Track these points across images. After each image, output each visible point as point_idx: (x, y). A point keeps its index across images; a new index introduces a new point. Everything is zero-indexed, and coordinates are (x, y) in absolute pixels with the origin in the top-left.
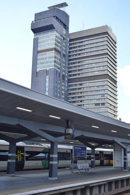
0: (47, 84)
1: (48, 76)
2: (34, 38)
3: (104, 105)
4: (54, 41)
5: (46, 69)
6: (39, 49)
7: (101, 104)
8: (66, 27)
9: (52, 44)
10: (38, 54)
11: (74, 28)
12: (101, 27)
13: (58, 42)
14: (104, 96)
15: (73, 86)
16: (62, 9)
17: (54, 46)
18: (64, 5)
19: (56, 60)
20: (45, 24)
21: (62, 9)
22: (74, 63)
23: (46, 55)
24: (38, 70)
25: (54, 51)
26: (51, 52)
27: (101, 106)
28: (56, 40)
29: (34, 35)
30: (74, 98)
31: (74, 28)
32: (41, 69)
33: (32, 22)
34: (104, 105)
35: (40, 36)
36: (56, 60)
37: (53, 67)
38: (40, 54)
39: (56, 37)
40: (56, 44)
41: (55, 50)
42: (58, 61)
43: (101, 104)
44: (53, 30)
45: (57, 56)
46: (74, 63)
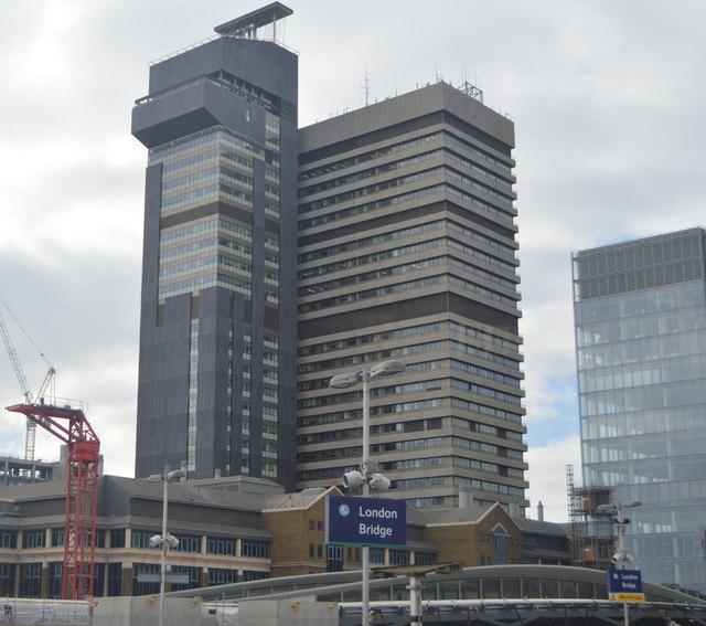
0: (194, 353)
1: (195, 322)
2: (145, 165)
3: (440, 427)
4: (217, 175)
5: (189, 290)
6: (167, 211)
7: (425, 423)
8: (285, 106)
9: (210, 189)
10: (163, 231)
11: (320, 100)
12: (418, 93)
13: (238, 176)
14: (439, 388)
15: (322, 351)
16: (263, 33)
17: (214, 196)
18: (276, 12)
19: (230, 250)
20: (216, 96)
21: (263, 33)
22: (324, 253)
23: (190, 236)
24: (162, 297)
25: (216, 216)
26: (207, 218)
27: (427, 433)
28: (224, 170)
29: (149, 154)
30: (328, 401)
31: (320, 100)
32: (206, 286)
33: (137, 102)
34: (440, 427)
35: (168, 157)
36: (230, 250)
37: (215, 283)
38: (169, 230)
39: (224, 155)
40: (224, 187)
41: (223, 208)
42: (241, 253)
43: (425, 423)
44: (214, 131)
45: (232, 233)
46: (324, 253)
